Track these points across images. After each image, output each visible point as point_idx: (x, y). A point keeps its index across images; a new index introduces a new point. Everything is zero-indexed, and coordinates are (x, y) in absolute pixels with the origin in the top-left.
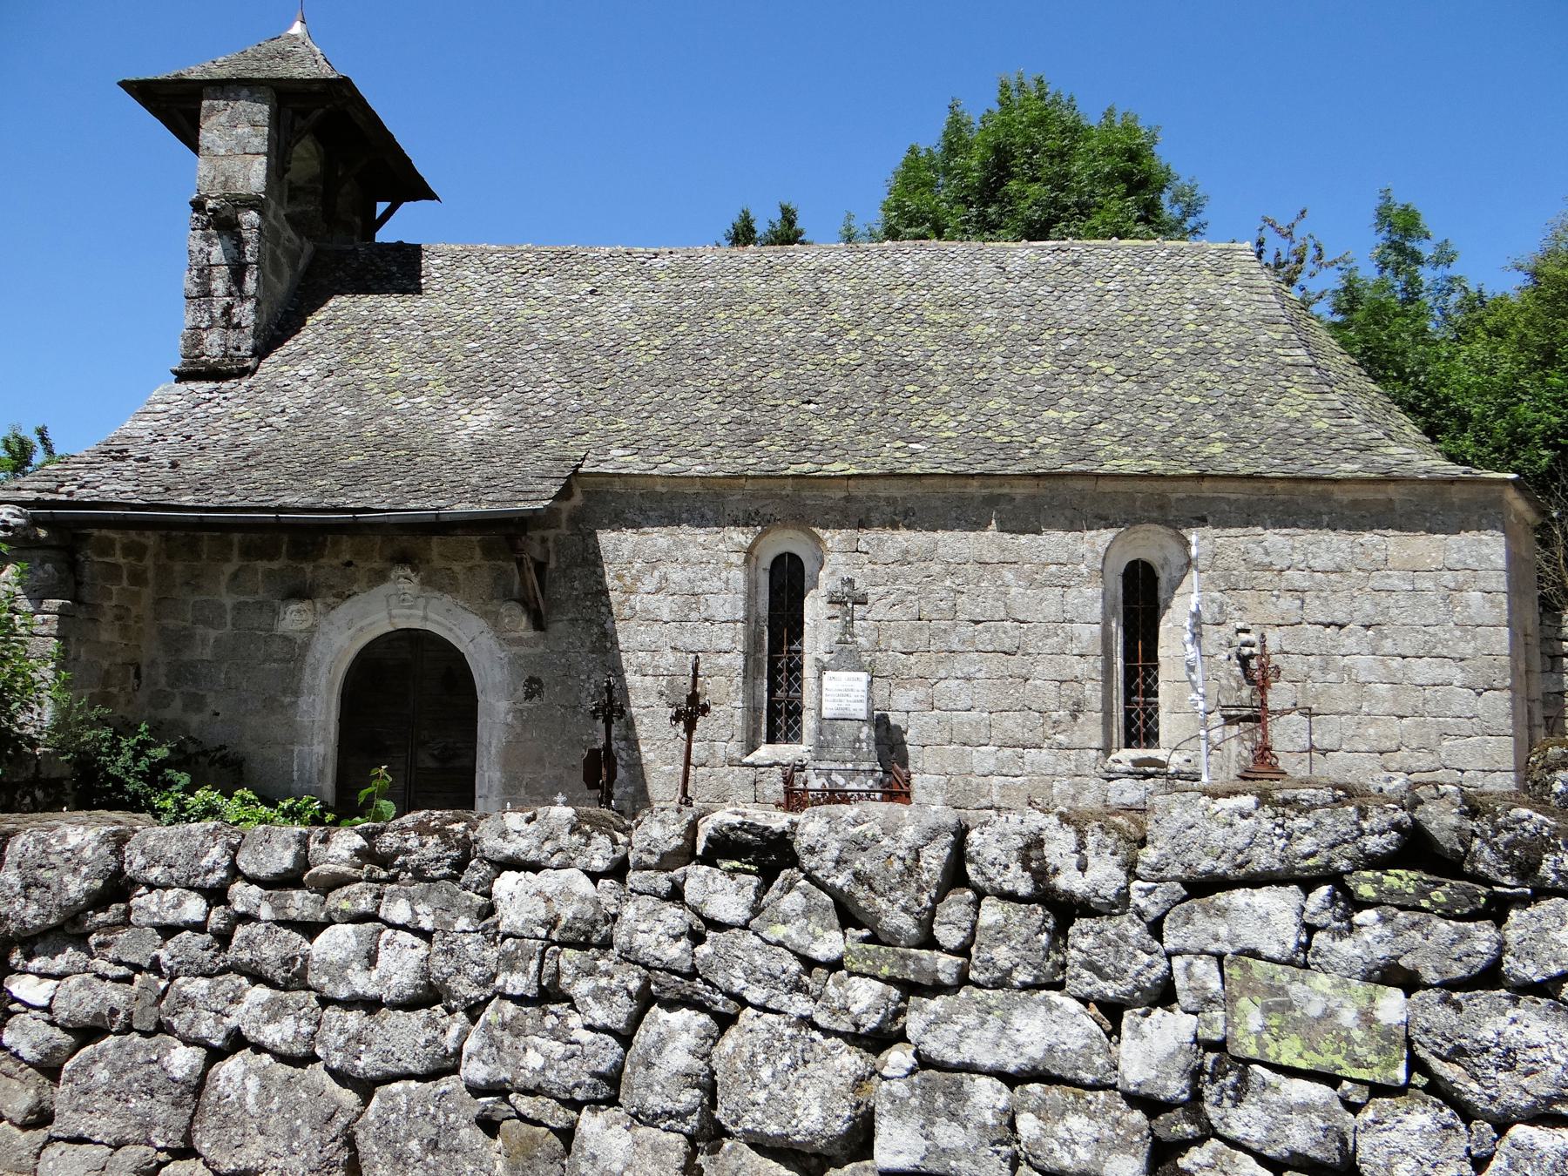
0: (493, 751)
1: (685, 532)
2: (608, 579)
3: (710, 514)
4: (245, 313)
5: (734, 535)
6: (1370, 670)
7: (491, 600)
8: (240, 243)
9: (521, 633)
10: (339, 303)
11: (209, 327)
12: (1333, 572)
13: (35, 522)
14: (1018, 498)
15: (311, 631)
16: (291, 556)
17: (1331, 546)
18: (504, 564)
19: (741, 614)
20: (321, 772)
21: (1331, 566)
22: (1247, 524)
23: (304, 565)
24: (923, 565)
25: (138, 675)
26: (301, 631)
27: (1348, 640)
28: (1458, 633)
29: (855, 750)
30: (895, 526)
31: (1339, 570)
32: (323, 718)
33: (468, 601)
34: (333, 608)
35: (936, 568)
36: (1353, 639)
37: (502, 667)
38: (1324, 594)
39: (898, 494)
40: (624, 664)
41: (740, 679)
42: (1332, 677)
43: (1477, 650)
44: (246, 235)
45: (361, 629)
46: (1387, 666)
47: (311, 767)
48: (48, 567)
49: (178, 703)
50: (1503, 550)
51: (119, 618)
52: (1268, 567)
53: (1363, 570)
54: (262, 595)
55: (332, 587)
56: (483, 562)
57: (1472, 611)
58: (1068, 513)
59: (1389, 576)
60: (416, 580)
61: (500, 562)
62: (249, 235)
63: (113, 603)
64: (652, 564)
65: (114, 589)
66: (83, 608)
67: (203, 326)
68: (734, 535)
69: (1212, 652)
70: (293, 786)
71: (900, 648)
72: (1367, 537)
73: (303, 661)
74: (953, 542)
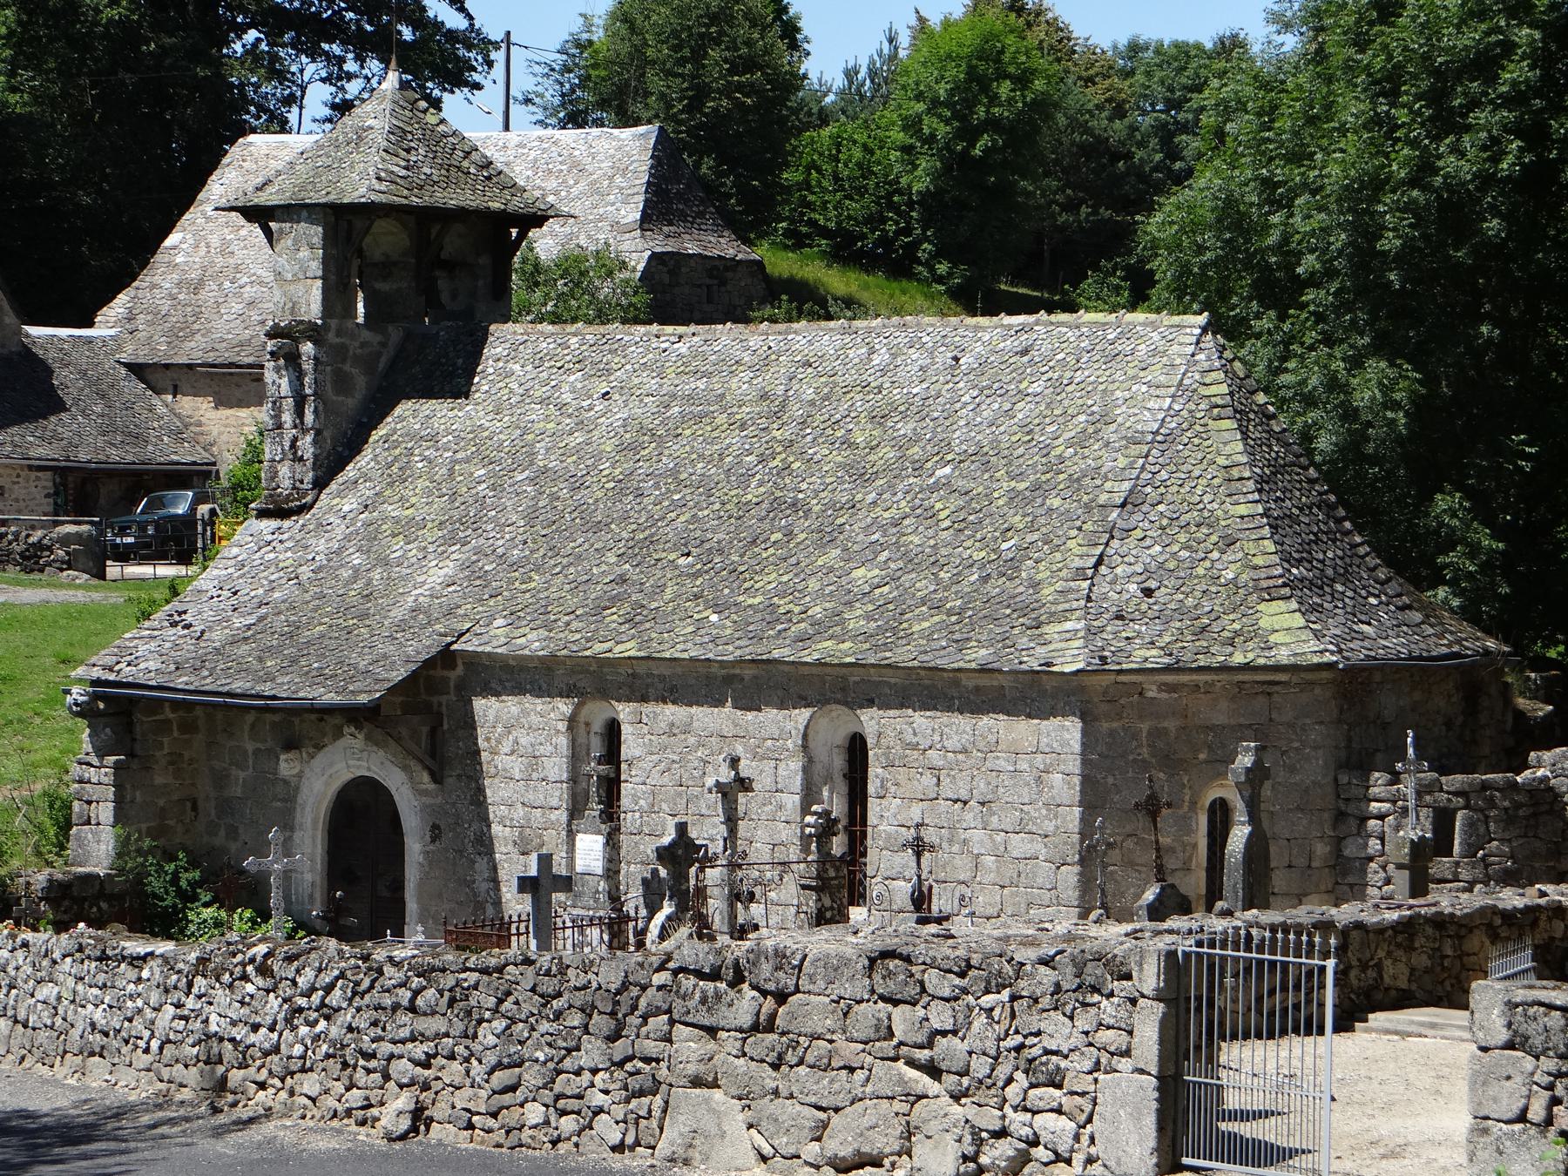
1: (529, 701)
2: (480, 741)
3: (545, 686)
4: (306, 445)
5: (560, 705)
6: (981, 842)
8: (300, 374)
10: (404, 408)
11: (282, 460)
12: (961, 752)
13: (95, 697)
14: (746, 678)
15: (300, 775)
17: (959, 728)
19: (565, 776)
20: (311, 896)
21: (959, 747)
22: (902, 706)
24: (683, 736)
25: (195, 808)
27: (970, 816)
28: (1044, 812)
29: (596, 900)
30: (665, 702)
31: (965, 751)
35: (692, 740)
36: (972, 814)
38: (953, 773)
39: (667, 673)
40: (491, 816)
41: (564, 833)
42: (956, 848)
43: (1057, 828)
44: (305, 366)
46: (993, 841)
48: (108, 730)
49: (222, 833)
50: (1078, 736)
51: (171, 763)
52: (915, 747)
53: (982, 752)
54: (270, 744)
57: (1055, 791)
58: (780, 692)
59: (998, 758)
62: (308, 366)
63: (166, 751)
64: (508, 729)
65: (166, 740)
66: (136, 760)
67: (277, 458)
68: (560, 705)
69: (876, 822)
71: (667, 810)
72: (986, 721)
73: (296, 802)
74: (703, 715)
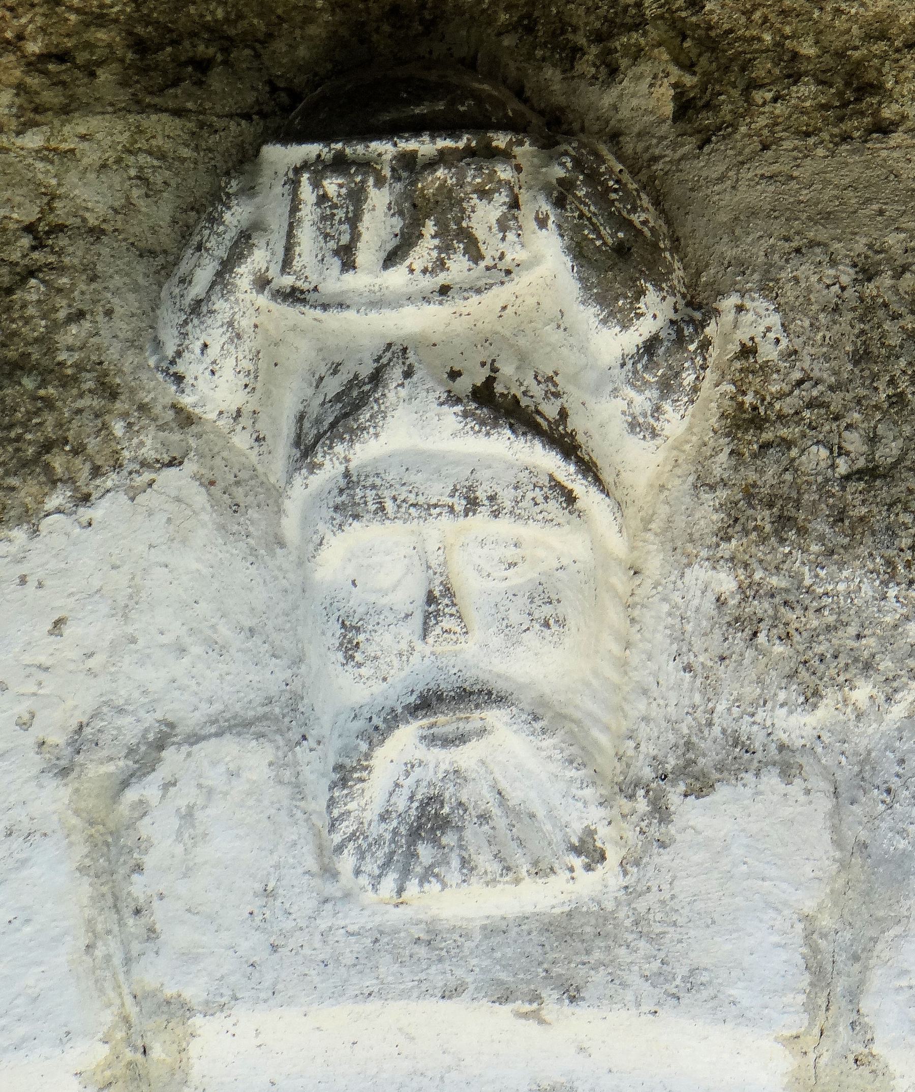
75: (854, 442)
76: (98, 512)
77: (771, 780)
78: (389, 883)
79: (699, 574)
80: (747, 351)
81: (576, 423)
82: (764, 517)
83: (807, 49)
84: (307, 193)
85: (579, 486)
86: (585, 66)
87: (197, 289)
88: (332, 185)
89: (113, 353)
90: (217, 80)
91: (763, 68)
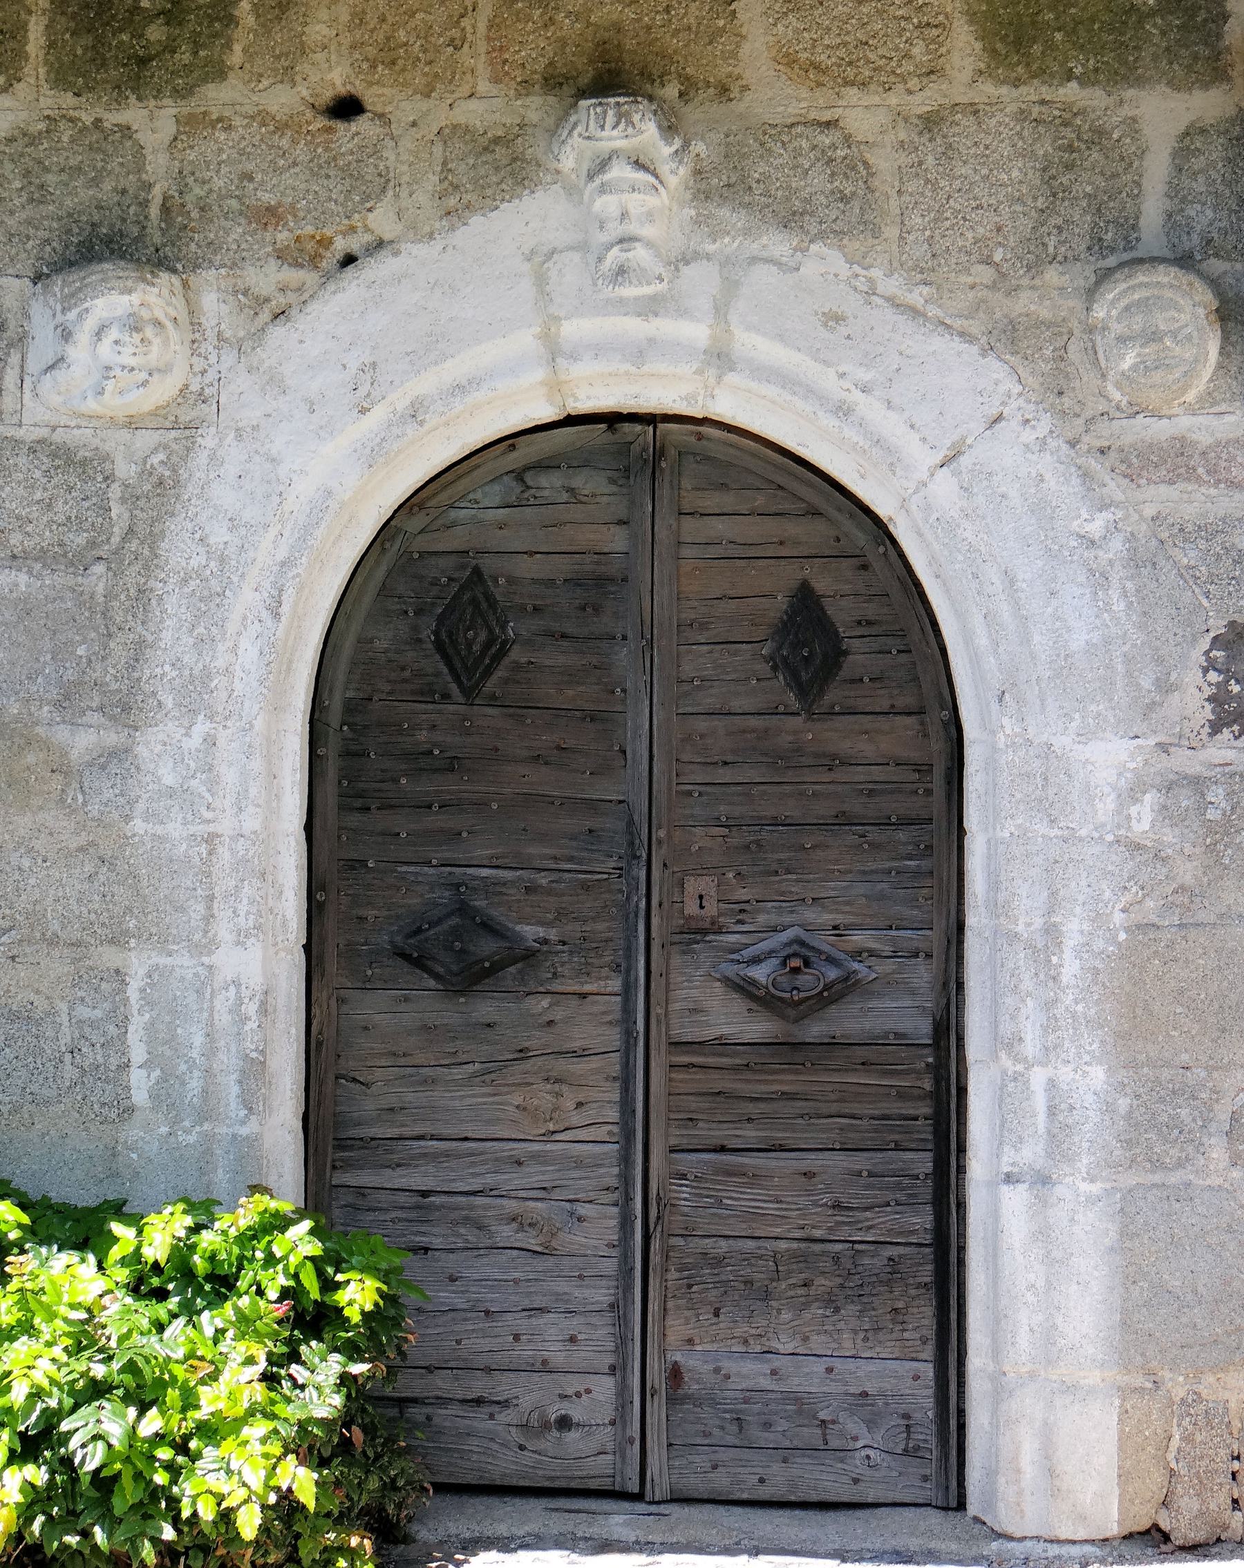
0: (1070, 968)
7: (1034, 268)
9: (1185, 422)
16: (61, 77)
18: (1091, 98)
23: (132, 114)
26: (132, 424)
32: (251, 823)
33: (923, 273)
34: (279, 315)
37: (1098, 578)
45: (415, 413)
47: (210, 1051)
55: (270, 216)
56: (988, 89)
60: (676, 176)
61: (1071, 91)
70: (133, 1132)
75: (724, 178)
76: (536, 195)
77: (705, 261)
78: (611, 287)
79: (686, 210)
80: (698, 155)
81: (658, 171)
82: (702, 196)
83: (712, 80)
84: (592, 111)
85: (659, 186)
86: (657, 84)
87: (563, 137)
88: (599, 110)
89: (539, 156)
90: (565, 87)
91: (700, 85)
